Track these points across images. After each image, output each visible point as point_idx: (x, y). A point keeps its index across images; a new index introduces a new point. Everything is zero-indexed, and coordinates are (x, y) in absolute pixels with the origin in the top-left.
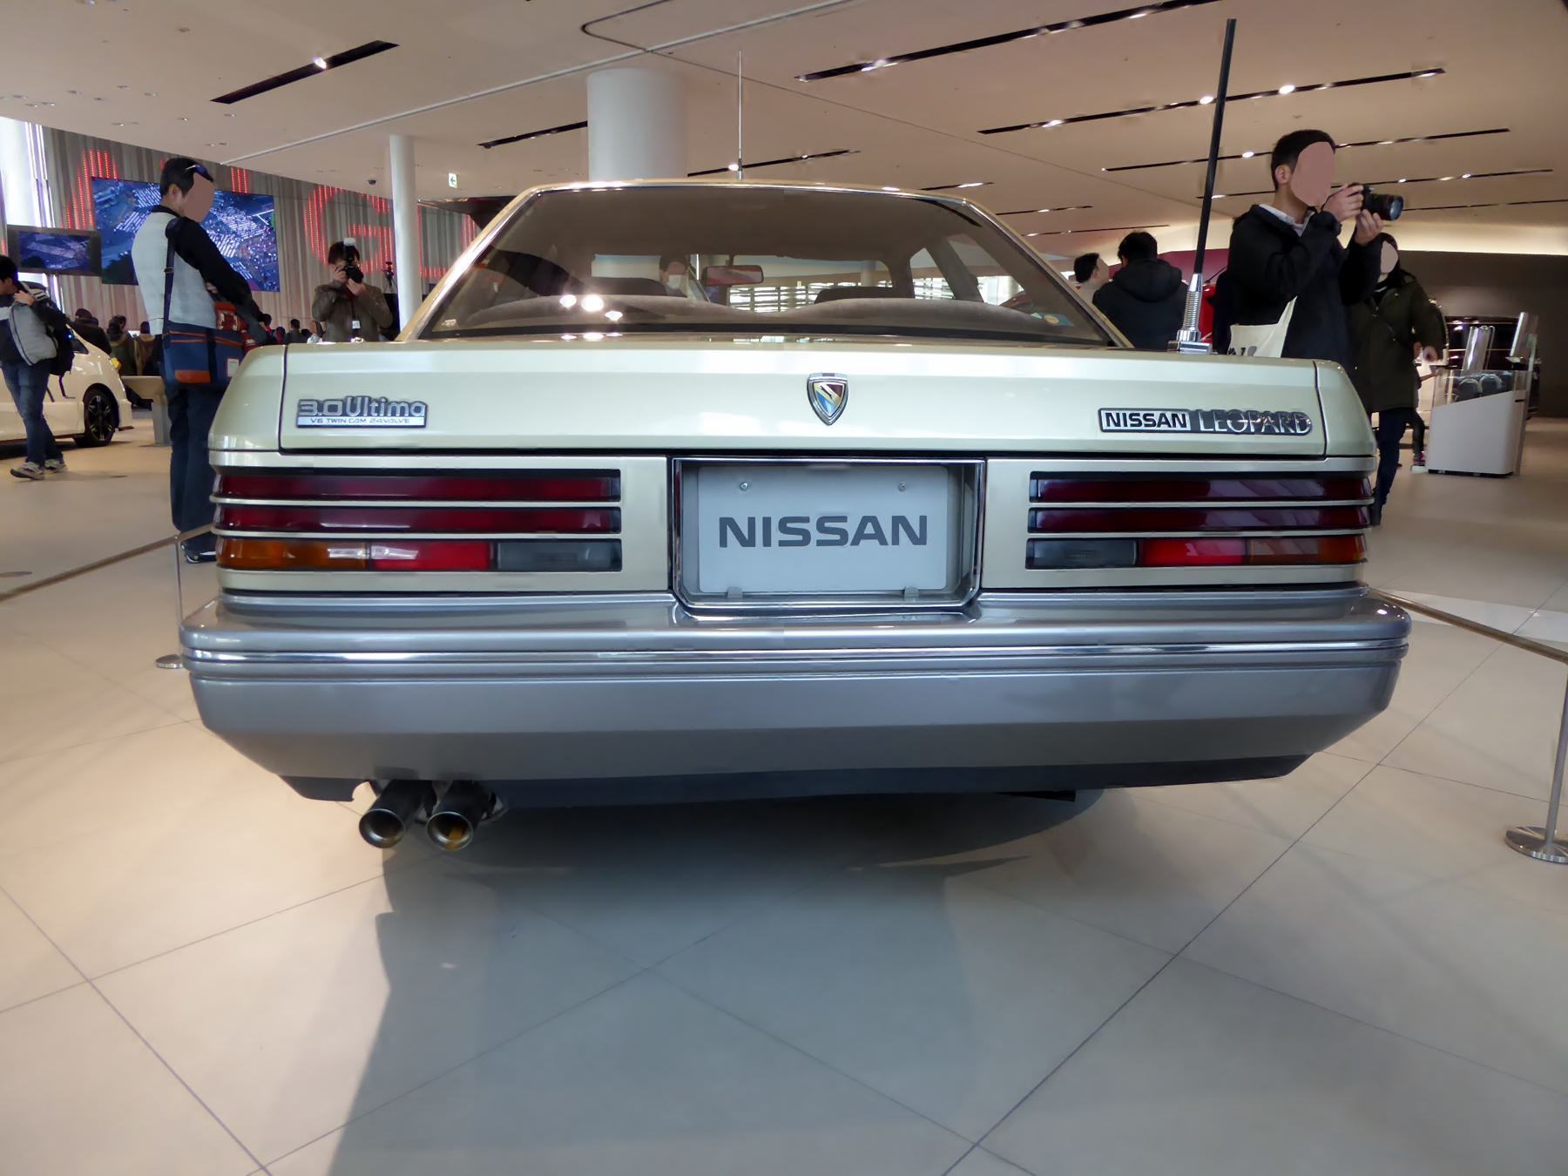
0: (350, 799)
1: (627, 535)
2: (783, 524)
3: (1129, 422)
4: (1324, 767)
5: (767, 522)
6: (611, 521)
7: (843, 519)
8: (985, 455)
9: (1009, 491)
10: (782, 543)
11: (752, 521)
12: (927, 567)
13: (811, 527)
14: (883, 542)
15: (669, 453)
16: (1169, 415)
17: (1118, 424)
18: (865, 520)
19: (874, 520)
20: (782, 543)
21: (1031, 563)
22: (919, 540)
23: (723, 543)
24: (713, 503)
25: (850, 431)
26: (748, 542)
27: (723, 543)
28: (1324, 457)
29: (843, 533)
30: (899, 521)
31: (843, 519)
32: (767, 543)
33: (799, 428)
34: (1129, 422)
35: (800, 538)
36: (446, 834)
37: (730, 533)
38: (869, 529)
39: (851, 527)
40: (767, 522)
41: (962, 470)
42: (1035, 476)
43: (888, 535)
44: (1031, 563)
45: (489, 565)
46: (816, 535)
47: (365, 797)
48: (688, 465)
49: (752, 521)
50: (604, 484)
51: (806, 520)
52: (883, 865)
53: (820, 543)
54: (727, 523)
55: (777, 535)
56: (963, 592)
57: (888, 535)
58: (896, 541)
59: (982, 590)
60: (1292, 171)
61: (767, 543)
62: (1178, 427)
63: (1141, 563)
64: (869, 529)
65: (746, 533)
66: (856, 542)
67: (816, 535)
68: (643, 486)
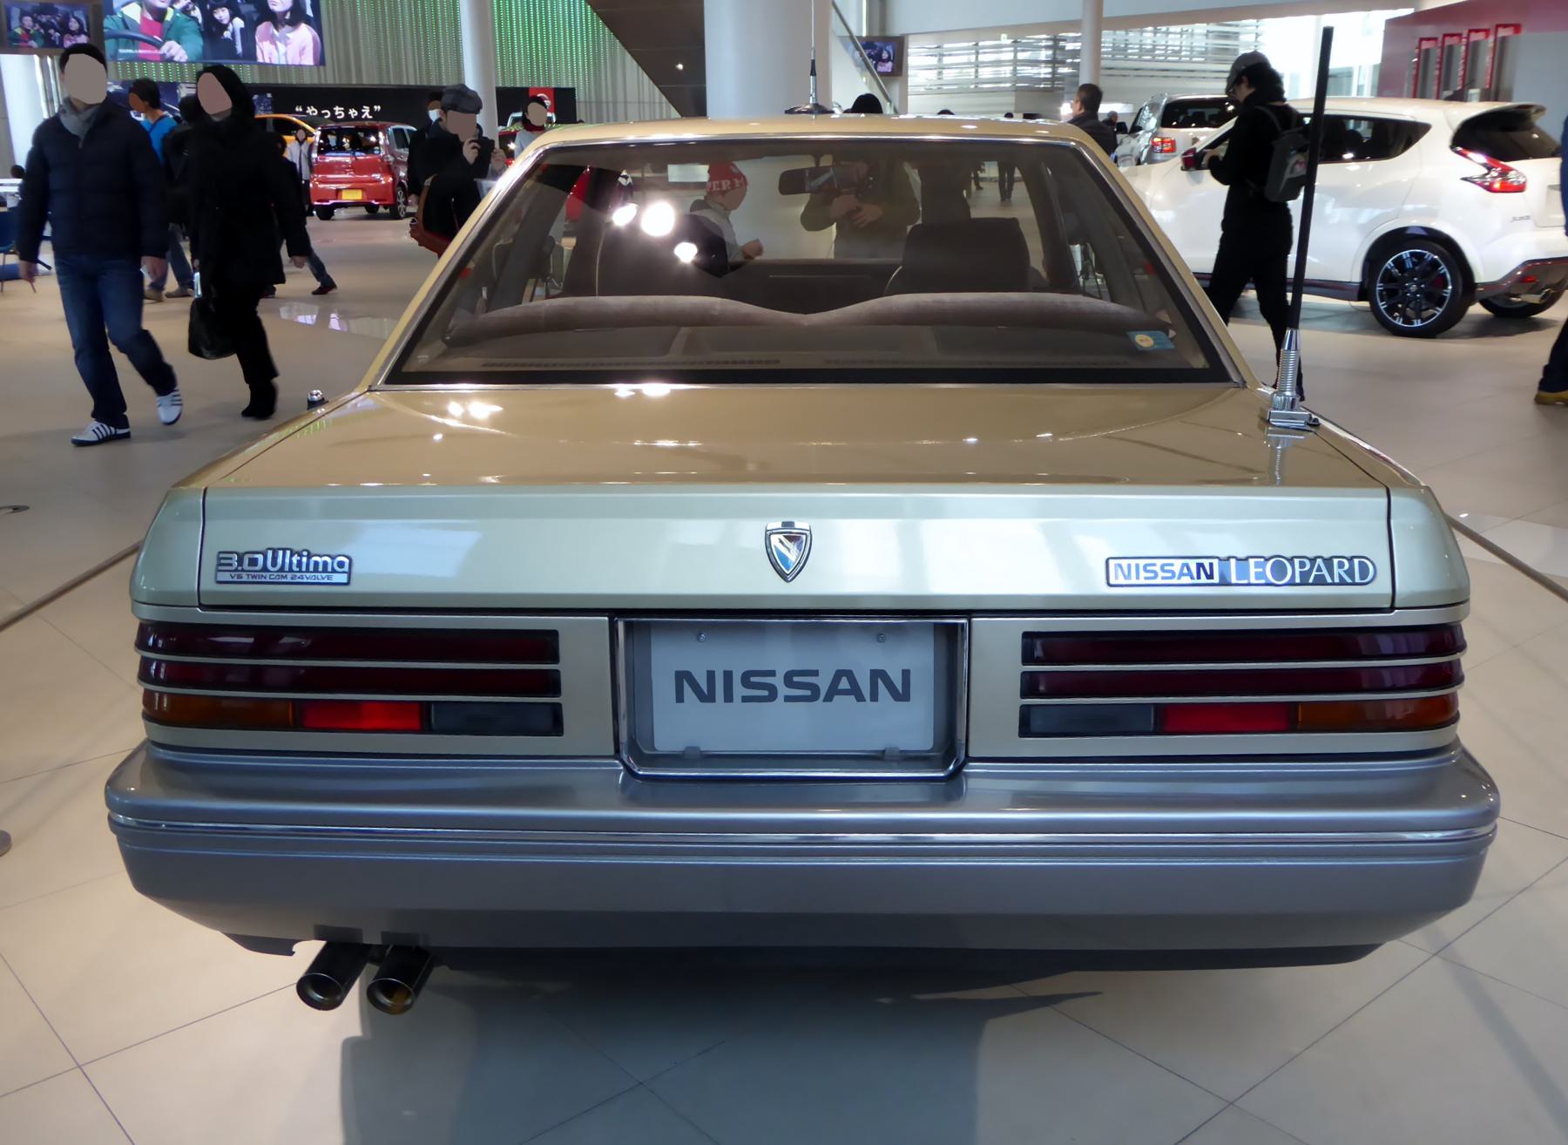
0: (292, 953)
1: (568, 699)
2: (746, 678)
3: (1143, 574)
4: (1398, 955)
5: (728, 675)
6: (551, 684)
7: (815, 673)
8: (969, 613)
9: (997, 659)
10: (745, 699)
11: (711, 675)
12: (912, 724)
13: (778, 681)
14: (860, 698)
15: (614, 613)
16: (1193, 564)
17: (1127, 577)
18: (839, 674)
19: (849, 674)
20: (745, 699)
21: (1026, 730)
22: (902, 695)
23: (680, 699)
24: (669, 657)
25: (815, 584)
26: (707, 697)
27: (680, 699)
28: (1392, 608)
29: (815, 689)
30: (878, 675)
31: (815, 673)
32: (729, 697)
33: (763, 585)
34: (1143, 574)
35: (766, 693)
36: (390, 997)
37: (687, 688)
38: (844, 684)
39: (823, 683)
40: (728, 675)
41: (947, 626)
42: (1028, 636)
43: (866, 692)
44: (1026, 730)
45: (425, 727)
46: (783, 691)
47: (308, 951)
48: (638, 621)
49: (711, 675)
50: (544, 645)
51: (772, 673)
52: (921, 997)
53: (788, 699)
54: (683, 677)
55: (739, 690)
56: (947, 760)
57: (866, 692)
58: (874, 697)
59: (969, 759)
60: (1540, 110)
61: (729, 697)
62: (1204, 580)
63: (1160, 730)
64: (844, 684)
65: (704, 686)
66: (829, 698)
67: (783, 691)
68: (583, 657)
